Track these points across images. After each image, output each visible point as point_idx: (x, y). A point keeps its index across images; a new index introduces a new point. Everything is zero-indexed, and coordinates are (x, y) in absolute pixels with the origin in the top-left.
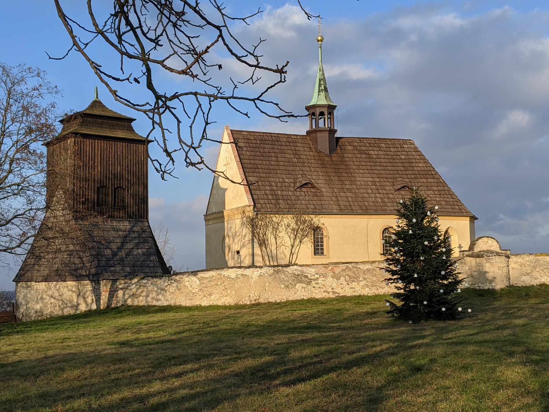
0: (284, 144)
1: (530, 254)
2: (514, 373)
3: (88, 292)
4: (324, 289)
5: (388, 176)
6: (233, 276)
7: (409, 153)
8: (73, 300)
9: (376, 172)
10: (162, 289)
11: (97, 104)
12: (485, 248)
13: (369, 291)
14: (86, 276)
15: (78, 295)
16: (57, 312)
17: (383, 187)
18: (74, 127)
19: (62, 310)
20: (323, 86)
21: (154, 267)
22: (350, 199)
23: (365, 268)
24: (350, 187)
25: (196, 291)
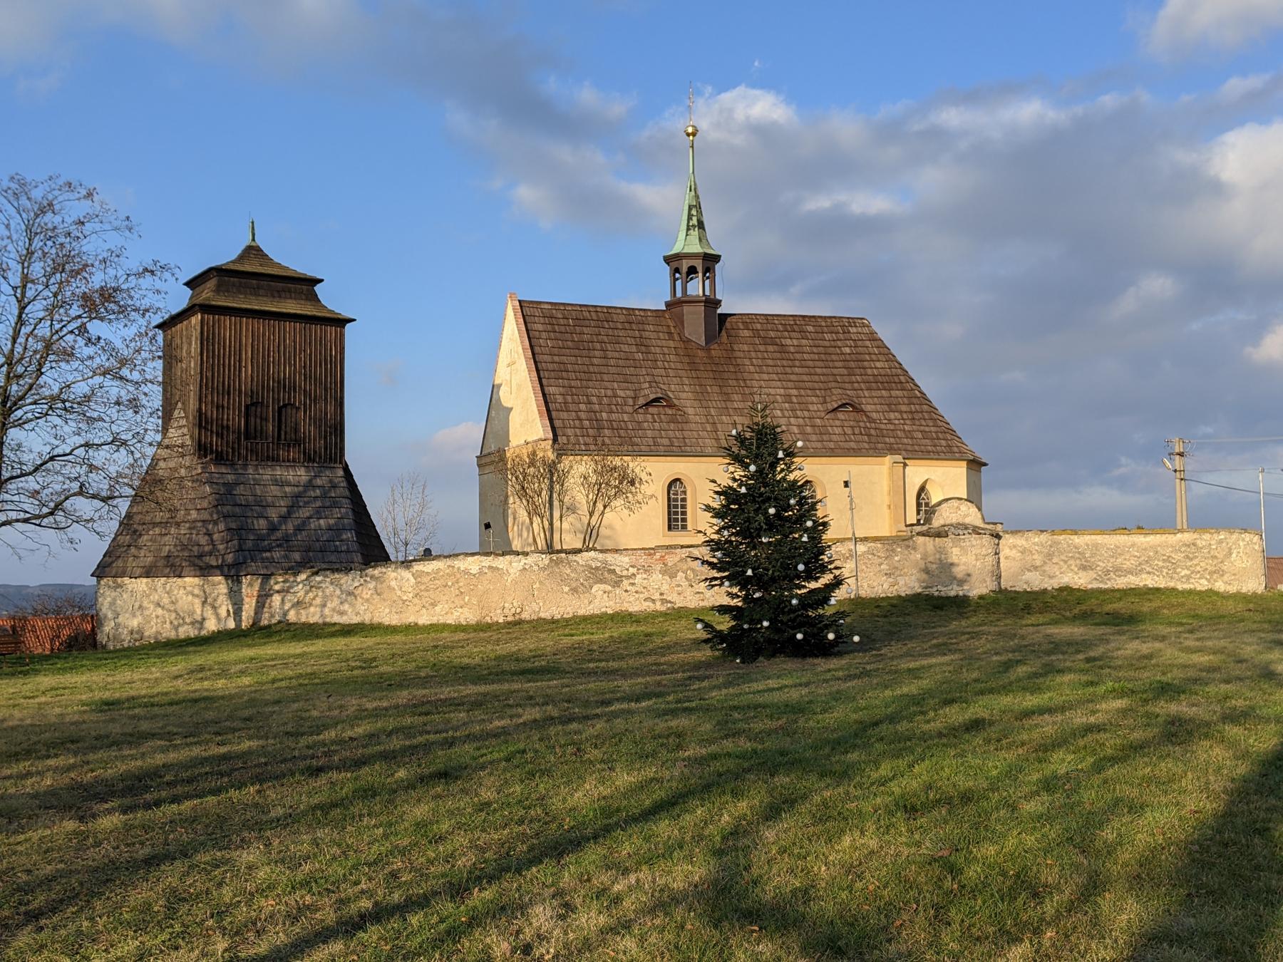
2: (280, 811)
3: (221, 597)
4: (646, 595)
6: (474, 569)
8: (194, 612)
9: (793, 377)
10: (350, 594)
11: (253, 251)
12: (954, 519)
14: (217, 567)
15: (204, 603)
16: (168, 633)
17: (804, 406)
18: (207, 293)
19: (176, 628)
20: (695, 219)
21: (348, 551)
25: (401, 599)
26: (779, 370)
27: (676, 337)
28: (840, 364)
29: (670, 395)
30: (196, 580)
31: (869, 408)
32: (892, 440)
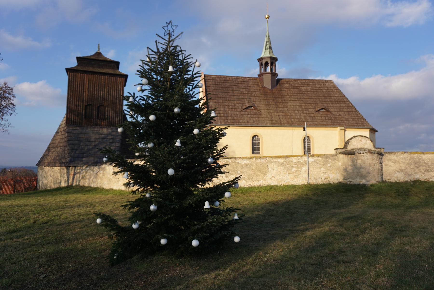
0: (240, 82)
1: (405, 152)
5: (312, 102)
7: (329, 88)
9: (304, 100)
13: (245, 184)
22: (281, 117)
23: (243, 163)
24: (282, 109)
26: (298, 97)
27: (261, 86)
28: (322, 95)
29: (256, 105)
30: (59, 168)
31: (332, 110)
32: (340, 121)
